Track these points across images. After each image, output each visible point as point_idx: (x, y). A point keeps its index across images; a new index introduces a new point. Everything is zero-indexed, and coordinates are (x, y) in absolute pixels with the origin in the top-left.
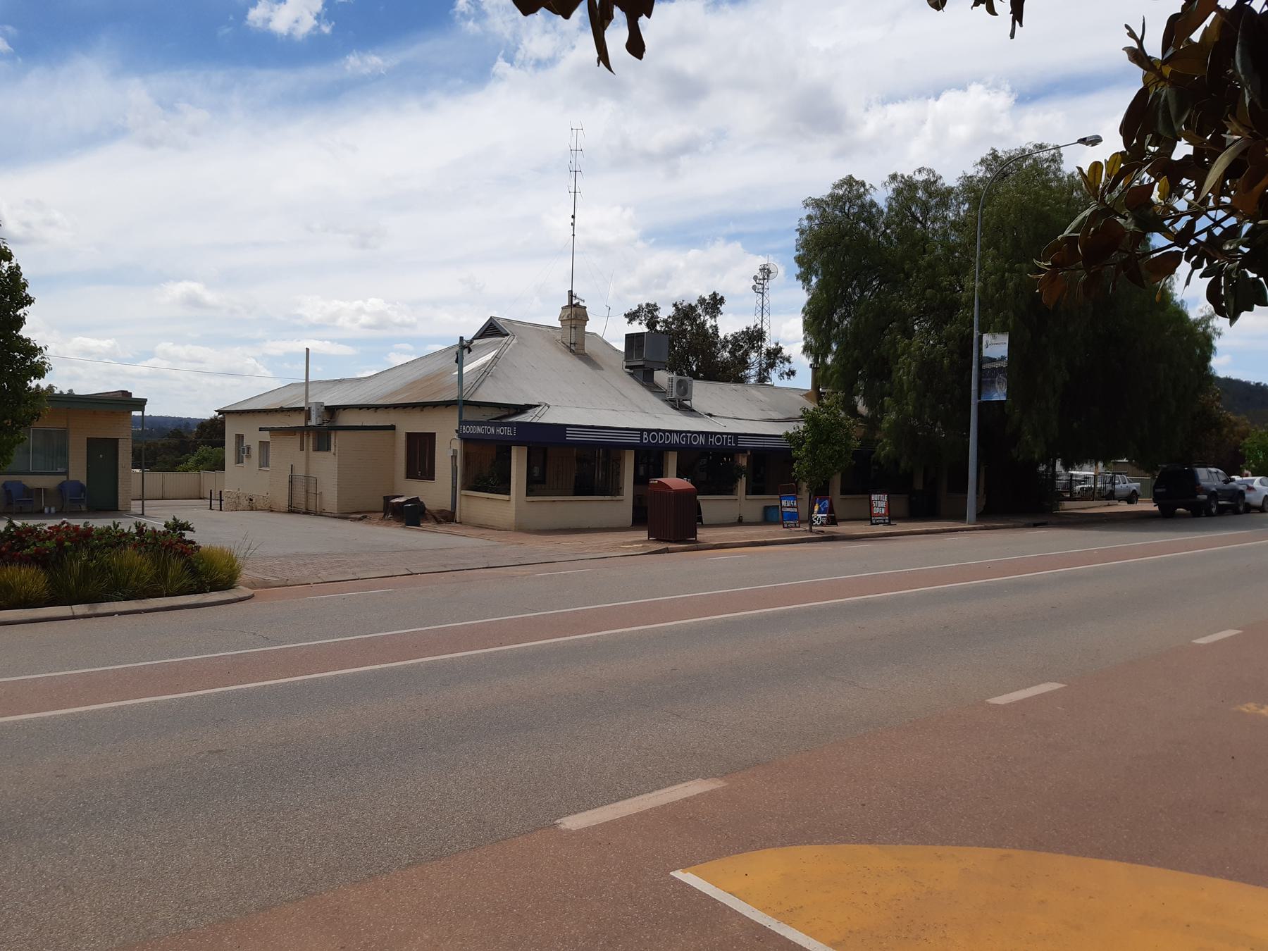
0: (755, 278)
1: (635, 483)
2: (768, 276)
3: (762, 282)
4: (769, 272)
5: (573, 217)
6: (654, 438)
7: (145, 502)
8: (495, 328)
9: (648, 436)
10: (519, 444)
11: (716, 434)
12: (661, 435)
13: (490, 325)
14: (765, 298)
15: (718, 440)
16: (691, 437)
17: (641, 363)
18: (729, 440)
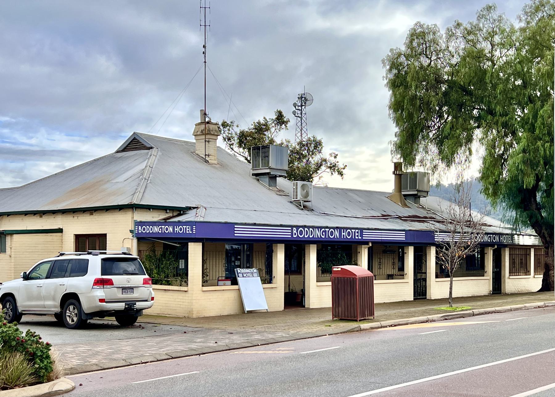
0: (295, 105)
1: (286, 272)
2: (305, 103)
3: (300, 108)
4: (306, 100)
5: (204, 47)
6: (301, 233)
7: (447, 296)
8: (138, 142)
9: (297, 232)
10: (195, 240)
11: (347, 228)
12: (307, 231)
13: (133, 140)
14: (303, 121)
15: (349, 233)
16: (328, 231)
17: (268, 171)
18: (357, 234)
